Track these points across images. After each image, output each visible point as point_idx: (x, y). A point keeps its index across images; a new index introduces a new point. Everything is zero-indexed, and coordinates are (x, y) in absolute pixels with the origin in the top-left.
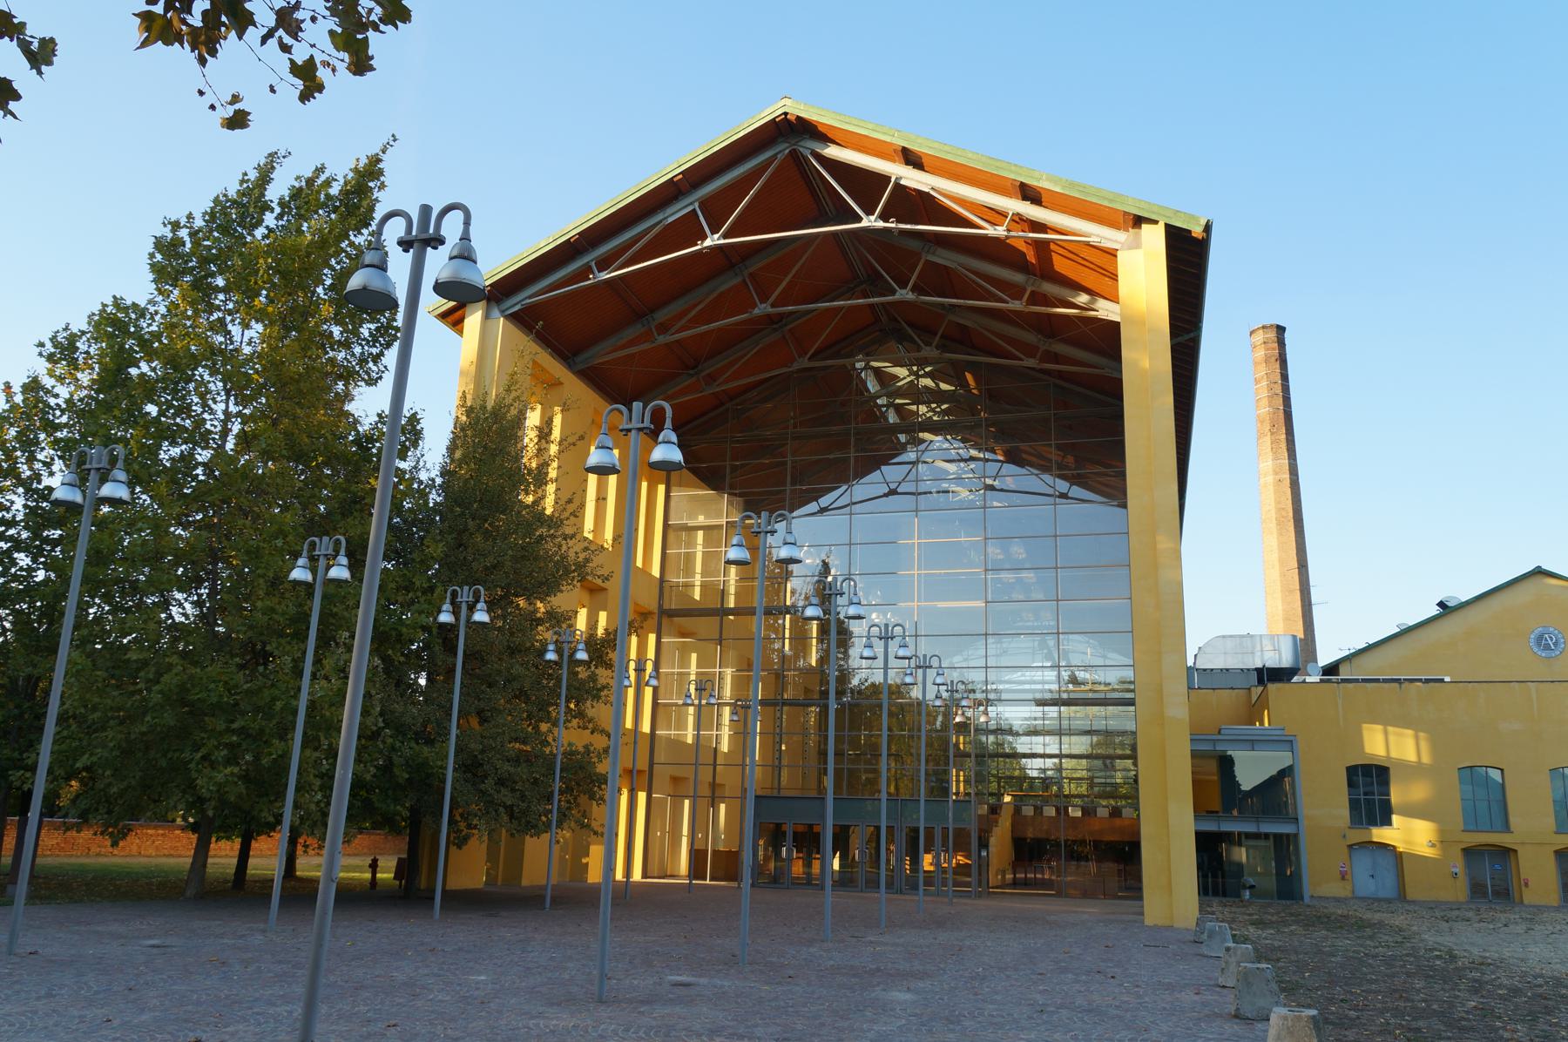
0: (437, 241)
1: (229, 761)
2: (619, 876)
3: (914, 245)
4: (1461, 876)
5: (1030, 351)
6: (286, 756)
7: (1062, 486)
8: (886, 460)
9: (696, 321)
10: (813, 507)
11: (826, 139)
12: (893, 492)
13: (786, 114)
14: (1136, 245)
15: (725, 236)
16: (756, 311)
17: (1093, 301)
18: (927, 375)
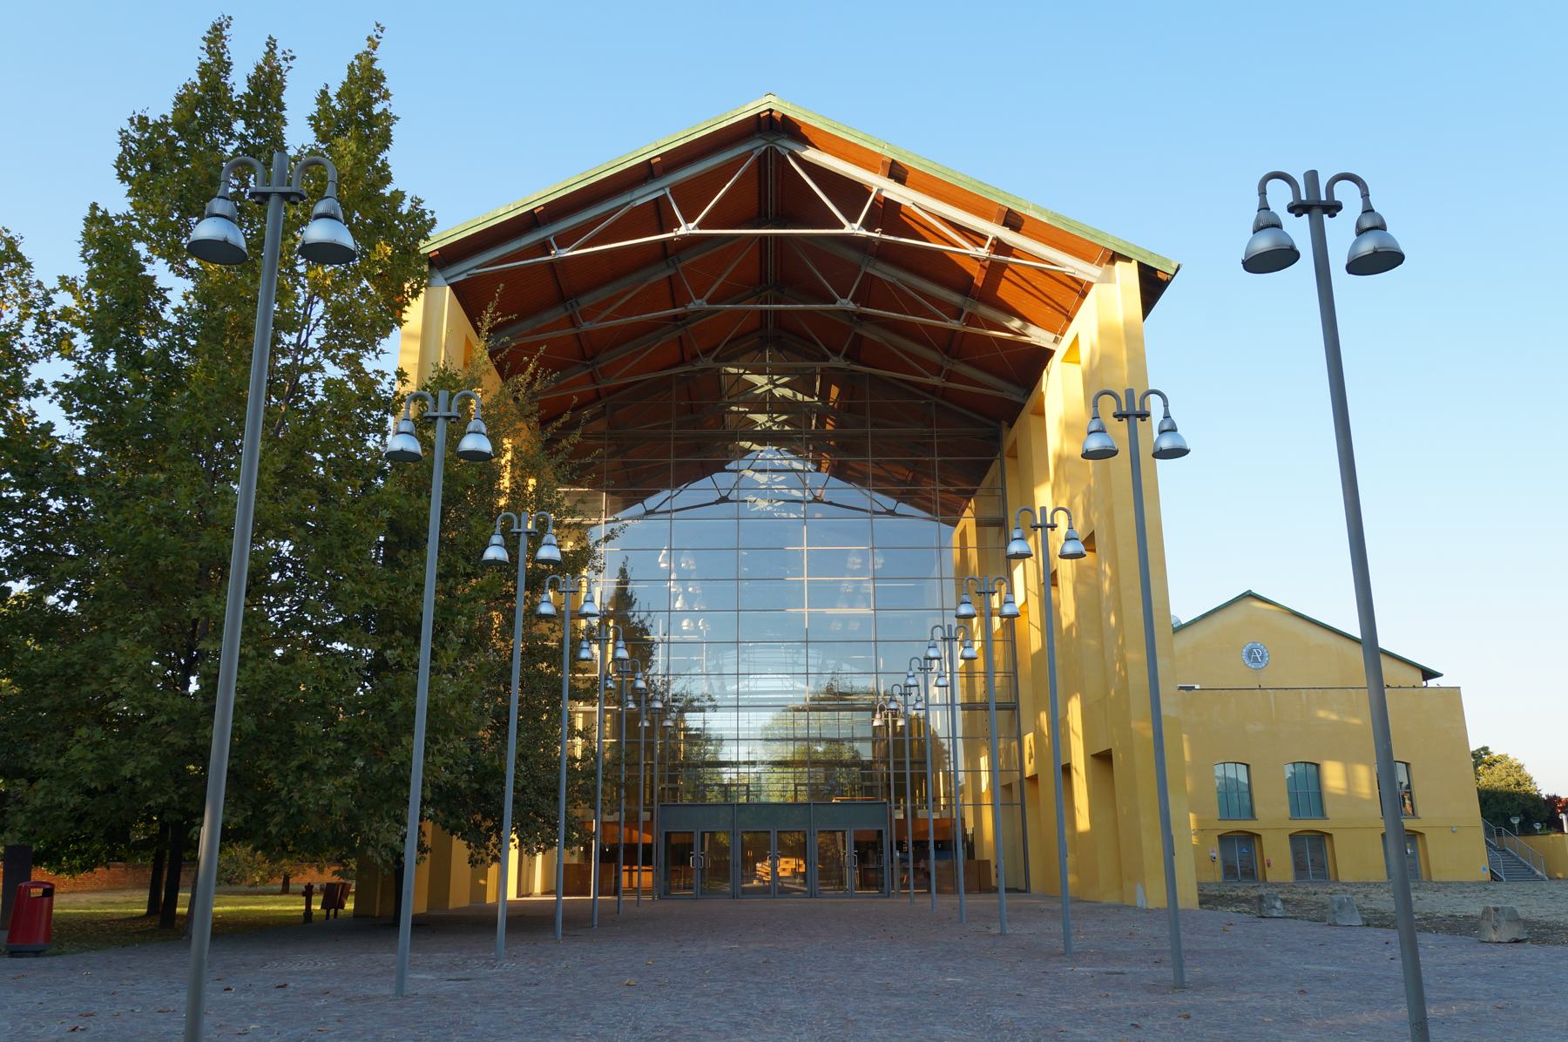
0: (1333, 208)
1: (334, 771)
2: (512, 894)
3: (853, 256)
4: (1218, 860)
5: (937, 370)
6: (406, 764)
7: (889, 503)
8: (721, 468)
9: (623, 312)
10: (638, 509)
11: (806, 142)
12: (724, 500)
13: (771, 110)
14: (1107, 279)
15: (700, 226)
16: (691, 306)
17: (1025, 327)
18: (784, 385)
